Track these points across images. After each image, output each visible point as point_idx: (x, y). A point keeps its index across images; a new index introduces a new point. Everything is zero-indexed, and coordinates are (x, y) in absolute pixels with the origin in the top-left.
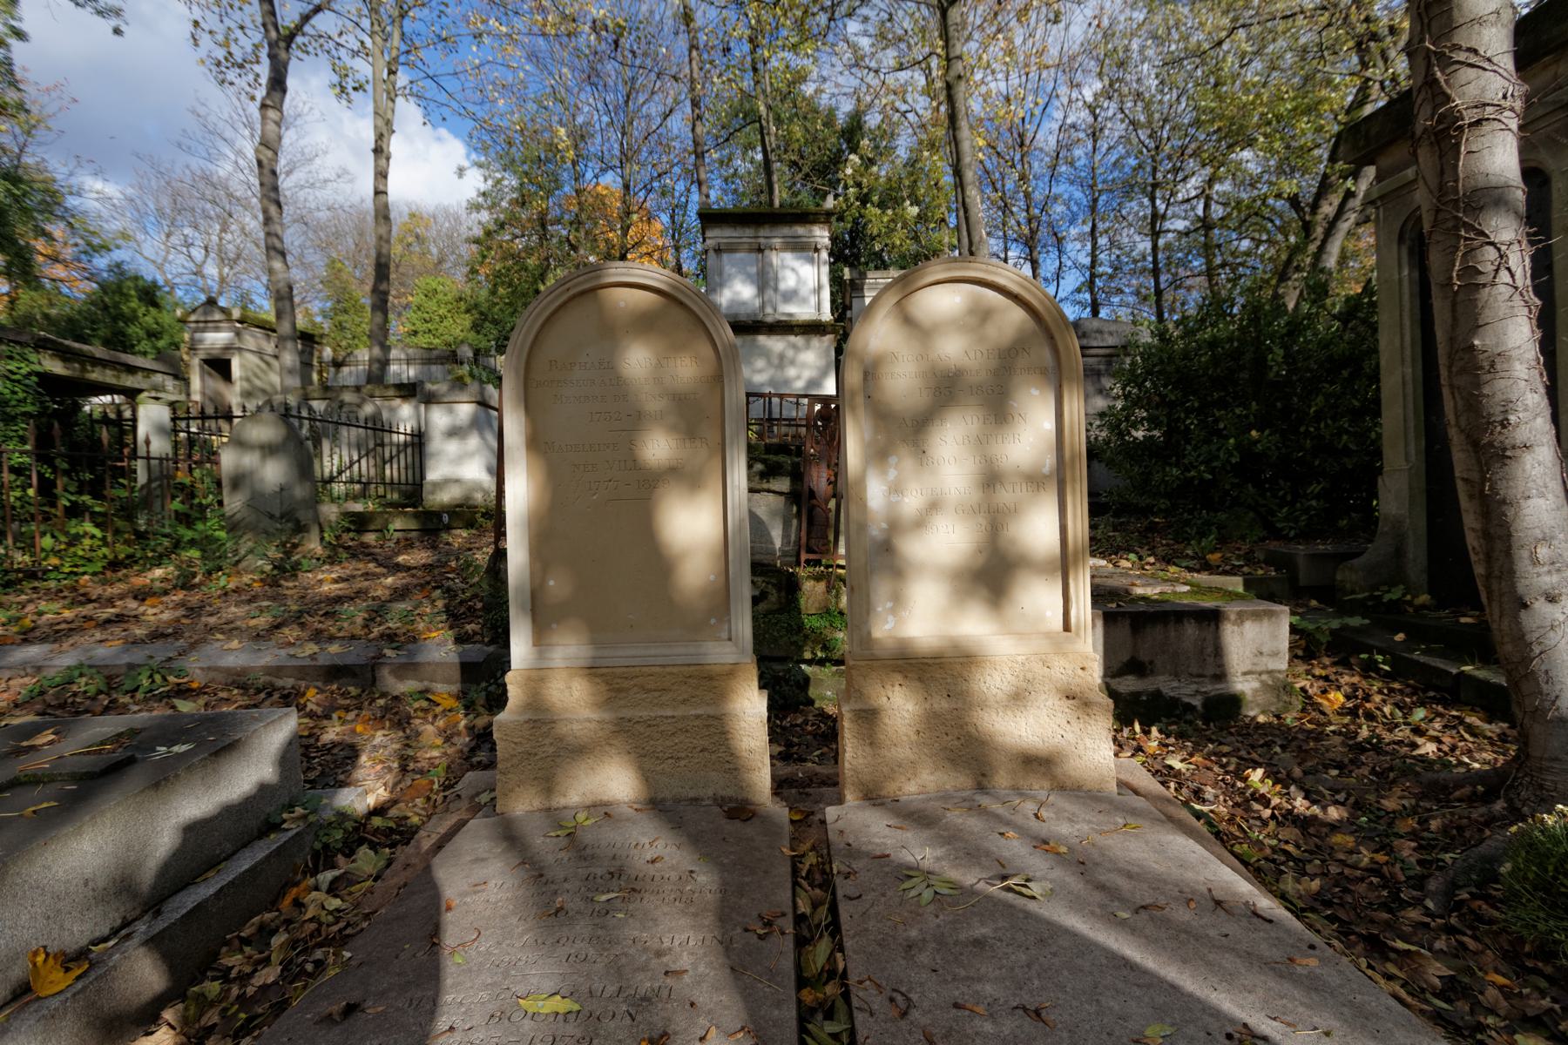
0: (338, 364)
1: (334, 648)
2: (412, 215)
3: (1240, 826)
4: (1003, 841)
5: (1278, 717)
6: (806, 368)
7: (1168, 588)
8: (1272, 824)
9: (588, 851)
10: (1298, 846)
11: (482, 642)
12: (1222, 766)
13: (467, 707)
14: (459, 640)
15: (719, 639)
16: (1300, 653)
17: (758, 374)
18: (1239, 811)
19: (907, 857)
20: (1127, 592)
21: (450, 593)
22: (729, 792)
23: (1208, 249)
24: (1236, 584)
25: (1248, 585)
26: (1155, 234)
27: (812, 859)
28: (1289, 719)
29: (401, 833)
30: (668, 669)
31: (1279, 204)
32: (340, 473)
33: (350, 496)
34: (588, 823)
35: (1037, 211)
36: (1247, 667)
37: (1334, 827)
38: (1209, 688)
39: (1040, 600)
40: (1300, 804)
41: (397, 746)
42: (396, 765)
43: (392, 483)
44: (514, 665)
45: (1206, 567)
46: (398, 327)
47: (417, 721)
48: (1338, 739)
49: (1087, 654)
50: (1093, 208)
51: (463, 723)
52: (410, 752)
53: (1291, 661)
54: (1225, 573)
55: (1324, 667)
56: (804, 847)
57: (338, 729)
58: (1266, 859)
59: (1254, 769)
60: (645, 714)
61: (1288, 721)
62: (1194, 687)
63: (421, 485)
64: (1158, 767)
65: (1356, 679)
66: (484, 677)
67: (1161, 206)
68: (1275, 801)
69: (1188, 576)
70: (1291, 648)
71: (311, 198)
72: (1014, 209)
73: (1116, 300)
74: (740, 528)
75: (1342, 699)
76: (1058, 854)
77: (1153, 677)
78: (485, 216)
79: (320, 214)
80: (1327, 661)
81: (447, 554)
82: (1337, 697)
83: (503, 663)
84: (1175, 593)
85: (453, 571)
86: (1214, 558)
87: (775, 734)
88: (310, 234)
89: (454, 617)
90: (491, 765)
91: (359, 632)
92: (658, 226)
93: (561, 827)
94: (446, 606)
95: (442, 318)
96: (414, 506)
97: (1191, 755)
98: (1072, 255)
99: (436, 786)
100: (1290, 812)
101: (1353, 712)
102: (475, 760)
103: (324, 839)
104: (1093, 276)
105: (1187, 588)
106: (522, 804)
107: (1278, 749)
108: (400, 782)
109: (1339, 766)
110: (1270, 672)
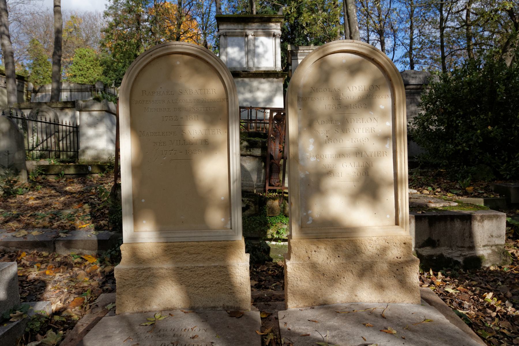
0: (35, 92)
1: (35, 233)
2: (73, 17)
5: (500, 267)
7: (447, 204)
8: (497, 320)
9: (162, 333)
10: (509, 331)
12: (473, 291)
14: (97, 229)
16: (511, 236)
18: (481, 313)
22: (231, 304)
24: (480, 202)
25: (486, 202)
26: (442, 29)
27: (271, 337)
28: (506, 268)
29: (69, 324)
30: (201, 243)
31: (504, 13)
33: (41, 157)
38: (467, 253)
40: (510, 310)
41: (67, 281)
42: (66, 290)
43: (63, 151)
45: (466, 194)
46: (65, 73)
50: (411, 16)
51: (99, 270)
54: (475, 196)
56: (267, 331)
57: (37, 273)
58: (494, 337)
59: (488, 293)
60: (189, 265)
61: (505, 269)
62: (459, 252)
63: (78, 152)
66: (110, 246)
67: (445, 14)
68: (498, 308)
69: (457, 198)
71: (22, 8)
72: (373, 16)
78: (111, 19)
83: (120, 241)
84: (450, 206)
85: (93, 195)
86: (470, 189)
87: (253, 275)
88: (22, 27)
90: (113, 290)
91: (46, 223)
93: (148, 321)
94: (91, 213)
95: (88, 69)
96: (74, 162)
97: (458, 286)
99: (86, 301)
100: (506, 314)
102: (105, 288)
103: (31, 327)
105: (456, 204)
106: (130, 308)
107: (500, 283)
110: (496, 245)
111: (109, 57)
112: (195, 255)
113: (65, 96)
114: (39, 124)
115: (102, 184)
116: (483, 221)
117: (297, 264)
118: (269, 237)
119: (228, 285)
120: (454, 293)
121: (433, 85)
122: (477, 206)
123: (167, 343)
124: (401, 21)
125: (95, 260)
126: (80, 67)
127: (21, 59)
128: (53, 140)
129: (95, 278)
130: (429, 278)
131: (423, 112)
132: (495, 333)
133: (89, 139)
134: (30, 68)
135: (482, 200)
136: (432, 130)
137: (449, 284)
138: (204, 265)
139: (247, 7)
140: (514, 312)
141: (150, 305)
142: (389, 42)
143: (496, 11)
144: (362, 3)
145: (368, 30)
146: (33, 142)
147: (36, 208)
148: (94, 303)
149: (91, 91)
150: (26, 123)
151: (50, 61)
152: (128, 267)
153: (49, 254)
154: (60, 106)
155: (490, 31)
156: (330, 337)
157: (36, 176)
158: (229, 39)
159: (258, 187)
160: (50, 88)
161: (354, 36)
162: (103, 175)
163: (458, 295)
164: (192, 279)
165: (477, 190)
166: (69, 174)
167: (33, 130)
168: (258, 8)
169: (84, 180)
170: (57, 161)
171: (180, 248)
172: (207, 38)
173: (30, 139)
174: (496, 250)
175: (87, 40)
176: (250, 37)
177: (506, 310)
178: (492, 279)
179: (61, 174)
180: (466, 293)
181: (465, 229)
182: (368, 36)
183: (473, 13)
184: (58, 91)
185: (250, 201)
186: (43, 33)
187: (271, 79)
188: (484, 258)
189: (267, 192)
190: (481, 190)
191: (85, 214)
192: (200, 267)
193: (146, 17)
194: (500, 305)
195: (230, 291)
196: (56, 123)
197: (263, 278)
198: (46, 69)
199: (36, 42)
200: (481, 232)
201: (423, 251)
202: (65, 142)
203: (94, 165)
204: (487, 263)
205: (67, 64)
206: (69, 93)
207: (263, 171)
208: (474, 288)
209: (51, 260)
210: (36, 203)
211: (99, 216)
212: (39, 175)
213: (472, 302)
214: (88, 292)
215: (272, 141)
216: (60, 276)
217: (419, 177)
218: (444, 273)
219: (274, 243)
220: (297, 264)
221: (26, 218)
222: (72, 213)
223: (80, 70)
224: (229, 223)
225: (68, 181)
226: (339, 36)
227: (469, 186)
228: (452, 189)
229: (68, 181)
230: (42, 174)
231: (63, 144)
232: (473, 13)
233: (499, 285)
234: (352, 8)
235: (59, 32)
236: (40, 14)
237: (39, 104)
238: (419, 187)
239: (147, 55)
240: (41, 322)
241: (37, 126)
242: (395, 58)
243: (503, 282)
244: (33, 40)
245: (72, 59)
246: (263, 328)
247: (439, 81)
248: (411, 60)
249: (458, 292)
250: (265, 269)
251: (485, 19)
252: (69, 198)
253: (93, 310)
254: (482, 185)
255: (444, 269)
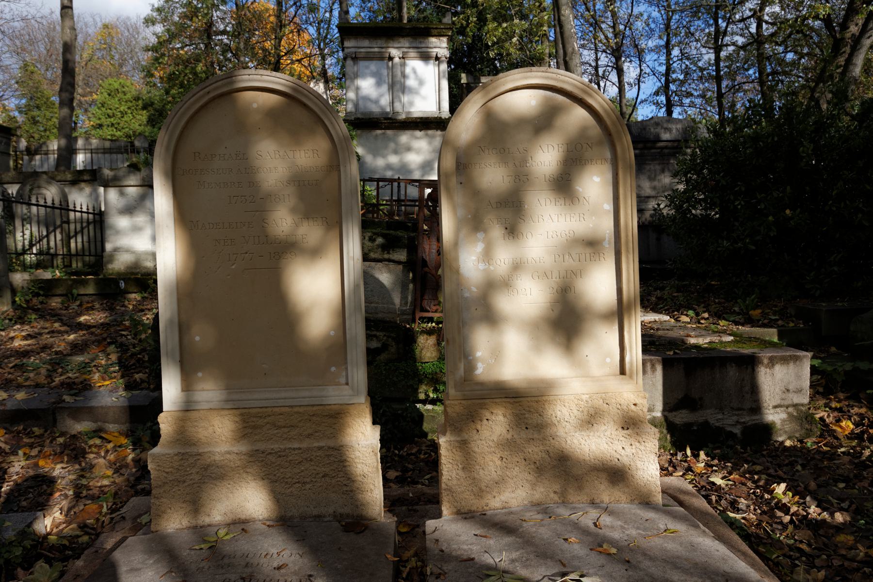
0: (31, 152)
1: (21, 395)
2: (106, 26)
3: (765, 530)
4: (566, 545)
5: (801, 441)
6: (417, 154)
7: (716, 339)
8: (791, 528)
9: (226, 561)
10: (809, 545)
11: (148, 389)
12: (754, 482)
13: (134, 444)
14: (128, 387)
15: (339, 384)
16: (821, 390)
17: (384, 162)
18: (766, 518)
19: (488, 560)
20: (683, 342)
21: (123, 348)
22: (347, 510)
23: (762, 58)
24: (772, 335)
25: (780, 336)
26: (718, 50)
27: (413, 563)
28: (809, 443)
29: (72, 549)
30: (296, 409)
31: (817, 23)
32: (31, 245)
33: (39, 265)
34: (228, 537)
35: (622, 27)
36: (777, 402)
37: (839, 529)
38: (748, 419)
39: (602, 344)
40: (813, 510)
41: (72, 477)
42: (71, 493)
43: (77, 255)
44: (165, 407)
45: (750, 321)
46: (84, 122)
47: (92, 456)
48: (847, 459)
49: (644, 393)
50: (667, 26)
51: (131, 457)
52: (84, 482)
53: (812, 398)
54: (764, 326)
55: (839, 402)
56: (407, 554)
57: (23, 463)
58: (784, 555)
59: (779, 484)
60: (276, 446)
61: (809, 444)
62: (735, 418)
63: (102, 257)
64: (703, 483)
65: (863, 410)
66: (143, 414)
67: (722, 24)
68: (794, 509)
69: (734, 328)
70: (811, 386)
71: (7, 10)
72: (603, 26)
73: (687, 101)
74: (356, 287)
75: (852, 426)
76: (609, 554)
77: (702, 407)
78: (159, 28)
79: (16, 24)
80: (841, 396)
81: (123, 314)
82: (848, 425)
83: (157, 405)
84: (721, 342)
85: (127, 329)
86: (756, 313)
87: (387, 462)
88: (7, 41)
89: (125, 368)
90: (147, 493)
91: (42, 380)
92: (306, 36)
93: (205, 541)
94: (120, 359)
95: (123, 114)
96: (95, 274)
97: (730, 473)
98: (650, 64)
99: (105, 510)
100: (805, 517)
101: (859, 437)
102: (140, 487)
103: (6, 556)
104: (667, 82)
105: (731, 338)
106: (174, 523)
107: (799, 468)
108: (74, 507)
109: (846, 480)
110: (795, 406)
111: (156, 94)
112: (286, 430)
113: (80, 159)
114: (34, 209)
115: (142, 310)
116: (773, 365)
117: (457, 441)
118: (422, 396)
119: (342, 479)
120: (723, 486)
121: (698, 141)
122: (765, 341)
123: (233, 577)
124: (650, 34)
125: (124, 441)
126: (109, 111)
127: (6, 97)
128: (59, 237)
129: (123, 471)
130: (686, 461)
131: (681, 187)
132: (787, 549)
133: (118, 232)
134: (20, 112)
135: (774, 331)
136: (695, 216)
137: (716, 471)
138: (301, 446)
139: (393, 9)
140: (819, 515)
141: (209, 515)
142: (632, 69)
143: (805, 18)
144: (585, 4)
145: (596, 51)
146: (24, 240)
147: (25, 354)
148: (118, 513)
149: (126, 152)
150: (11, 208)
151: (55, 99)
152: (171, 451)
153: (46, 431)
154: (69, 177)
155: (796, 53)
156: (507, 563)
157: (28, 298)
158: (362, 64)
159: (403, 313)
160: (56, 148)
161: (571, 59)
162: (146, 295)
163: (730, 489)
164: (282, 470)
165: (767, 314)
166: (86, 295)
167: (23, 220)
168: (412, 13)
169: (113, 304)
170: (65, 272)
171: (261, 417)
172: (327, 62)
173: (19, 235)
174: (795, 414)
175: (121, 66)
176: (397, 60)
177: (806, 511)
178: (787, 461)
179: (72, 295)
180: (744, 484)
181: (743, 380)
182: (597, 60)
183: (767, 22)
184: (67, 154)
185: (388, 337)
186: (45, 52)
187: (430, 132)
188: (775, 427)
189: (418, 321)
190: (774, 315)
191: (109, 362)
192: (294, 449)
193: (222, 27)
194: (797, 503)
195: (345, 489)
196: (64, 207)
197: (410, 466)
198: (48, 114)
199: (31, 68)
200: (770, 383)
201: (675, 416)
202: (79, 239)
203: (130, 279)
204: (781, 436)
205: (86, 106)
206: (89, 155)
207: (411, 286)
208: (756, 477)
209: (48, 441)
210: (26, 345)
211: (133, 365)
212: (33, 296)
213: (752, 499)
214: (108, 495)
215: (425, 237)
216: (63, 468)
217: (675, 294)
218: (710, 452)
219: (429, 407)
220: (457, 441)
221: (8, 370)
222: (87, 361)
223: (109, 117)
224: (344, 374)
225: (84, 306)
226: (547, 59)
227: (754, 309)
228: (727, 313)
229: (84, 306)
230: (37, 295)
231: (76, 242)
232: (767, 22)
233: (797, 471)
234: (567, 12)
235: (68, 48)
236: (39, 20)
237: (35, 175)
238: (673, 312)
239: (202, 93)
240: (23, 547)
241: (30, 212)
242: (642, 97)
243: (804, 466)
244: (26, 65)
245: (95, 96)
246: (398, 550)
247: (707, 135)
248: (668, 100)
249: (731, 483)
250: (414, 451)
251: (794, 31)
252: (84, 335)
253: (117, 526)
254: (776, 306)
255: (710, 445)
